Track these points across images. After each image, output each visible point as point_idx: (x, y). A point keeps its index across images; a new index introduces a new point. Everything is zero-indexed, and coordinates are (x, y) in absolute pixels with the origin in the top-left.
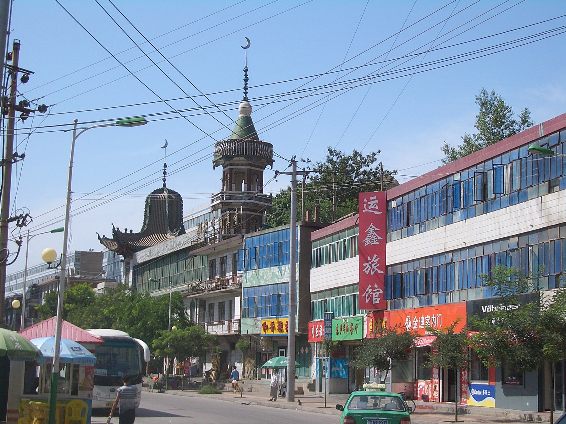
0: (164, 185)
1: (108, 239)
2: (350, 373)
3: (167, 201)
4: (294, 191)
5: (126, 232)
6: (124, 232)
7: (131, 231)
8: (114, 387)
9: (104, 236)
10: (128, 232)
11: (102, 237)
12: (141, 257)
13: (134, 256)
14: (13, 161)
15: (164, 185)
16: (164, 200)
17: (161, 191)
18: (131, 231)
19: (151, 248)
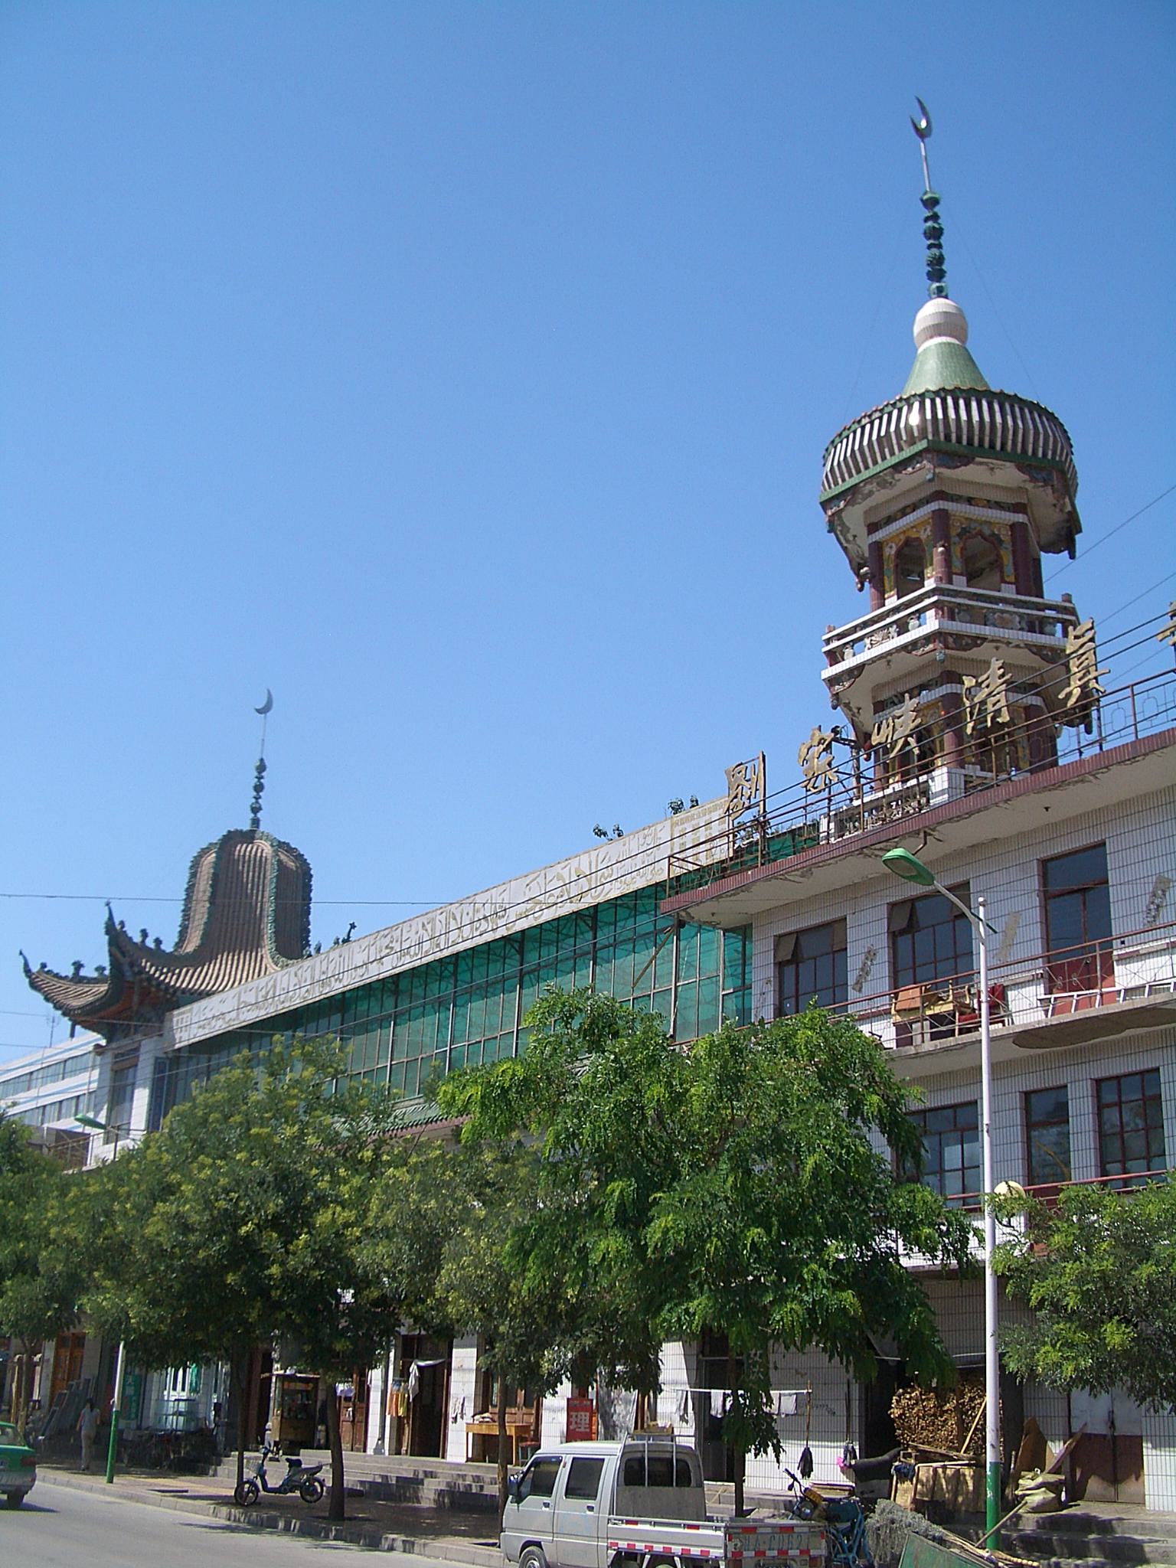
0: (256, 822)
1: (57, 975)
2: (1142, 948)
3: (271, 874)
4: (81, 1173)
5: (143, 941)
6: (137, 939)
7: (158, 942)
8: (1055, 1020)
9: (44, 966)
10: (150, 943)
11: (35, 968)
12: (192, 1025)
13: (167, 1024)
14: (281, 1525)
15: (256, 822)
16: (261, 863)
17: (249, 837)
18: (158, 942)
19: (216, 998)
